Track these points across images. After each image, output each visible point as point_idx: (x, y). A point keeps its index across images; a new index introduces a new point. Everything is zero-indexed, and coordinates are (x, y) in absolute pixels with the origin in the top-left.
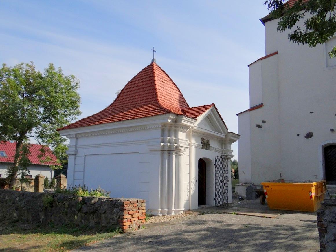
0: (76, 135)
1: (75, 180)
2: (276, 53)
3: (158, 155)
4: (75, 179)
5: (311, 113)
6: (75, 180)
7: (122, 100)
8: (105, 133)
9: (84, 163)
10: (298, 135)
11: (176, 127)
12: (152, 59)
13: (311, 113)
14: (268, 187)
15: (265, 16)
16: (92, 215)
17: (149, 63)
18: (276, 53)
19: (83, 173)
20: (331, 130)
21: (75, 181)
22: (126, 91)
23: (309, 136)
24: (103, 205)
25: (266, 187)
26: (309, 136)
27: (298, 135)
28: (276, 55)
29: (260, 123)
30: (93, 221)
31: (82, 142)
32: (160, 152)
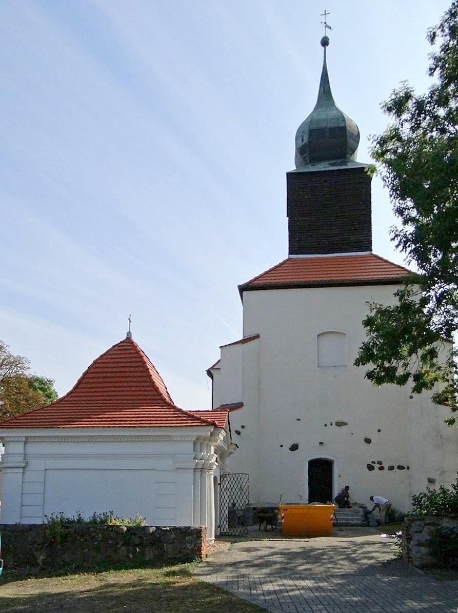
0: (26, 438)
1: (23, 505)
2: (257, 337)
3: (190, 475)
4: (23, 504)
5: (298, 420)
6: (23, 505)
7: (102, 390)
8: (91, 439)
9: (44, 482)
10: (282, 446)
11: (210, 440)
12: (128, 332)
13: (298, 420)
14: (287, 510)
15: (243, 283)
16: (150, 547)
17: (124, 338)
18: (257, 337)
19: (43, 495)
20: (320, 443)
21: (23, 507)
22: (91, 376)
23: (294, 448)
24: (168, 534)
25: (284, 510)
26: (294, 448)
27: (282, 446)
28: (256, 340)
29: (240, 429)
30: (150, 554)
31: (32, 449)
32: (192, 471)
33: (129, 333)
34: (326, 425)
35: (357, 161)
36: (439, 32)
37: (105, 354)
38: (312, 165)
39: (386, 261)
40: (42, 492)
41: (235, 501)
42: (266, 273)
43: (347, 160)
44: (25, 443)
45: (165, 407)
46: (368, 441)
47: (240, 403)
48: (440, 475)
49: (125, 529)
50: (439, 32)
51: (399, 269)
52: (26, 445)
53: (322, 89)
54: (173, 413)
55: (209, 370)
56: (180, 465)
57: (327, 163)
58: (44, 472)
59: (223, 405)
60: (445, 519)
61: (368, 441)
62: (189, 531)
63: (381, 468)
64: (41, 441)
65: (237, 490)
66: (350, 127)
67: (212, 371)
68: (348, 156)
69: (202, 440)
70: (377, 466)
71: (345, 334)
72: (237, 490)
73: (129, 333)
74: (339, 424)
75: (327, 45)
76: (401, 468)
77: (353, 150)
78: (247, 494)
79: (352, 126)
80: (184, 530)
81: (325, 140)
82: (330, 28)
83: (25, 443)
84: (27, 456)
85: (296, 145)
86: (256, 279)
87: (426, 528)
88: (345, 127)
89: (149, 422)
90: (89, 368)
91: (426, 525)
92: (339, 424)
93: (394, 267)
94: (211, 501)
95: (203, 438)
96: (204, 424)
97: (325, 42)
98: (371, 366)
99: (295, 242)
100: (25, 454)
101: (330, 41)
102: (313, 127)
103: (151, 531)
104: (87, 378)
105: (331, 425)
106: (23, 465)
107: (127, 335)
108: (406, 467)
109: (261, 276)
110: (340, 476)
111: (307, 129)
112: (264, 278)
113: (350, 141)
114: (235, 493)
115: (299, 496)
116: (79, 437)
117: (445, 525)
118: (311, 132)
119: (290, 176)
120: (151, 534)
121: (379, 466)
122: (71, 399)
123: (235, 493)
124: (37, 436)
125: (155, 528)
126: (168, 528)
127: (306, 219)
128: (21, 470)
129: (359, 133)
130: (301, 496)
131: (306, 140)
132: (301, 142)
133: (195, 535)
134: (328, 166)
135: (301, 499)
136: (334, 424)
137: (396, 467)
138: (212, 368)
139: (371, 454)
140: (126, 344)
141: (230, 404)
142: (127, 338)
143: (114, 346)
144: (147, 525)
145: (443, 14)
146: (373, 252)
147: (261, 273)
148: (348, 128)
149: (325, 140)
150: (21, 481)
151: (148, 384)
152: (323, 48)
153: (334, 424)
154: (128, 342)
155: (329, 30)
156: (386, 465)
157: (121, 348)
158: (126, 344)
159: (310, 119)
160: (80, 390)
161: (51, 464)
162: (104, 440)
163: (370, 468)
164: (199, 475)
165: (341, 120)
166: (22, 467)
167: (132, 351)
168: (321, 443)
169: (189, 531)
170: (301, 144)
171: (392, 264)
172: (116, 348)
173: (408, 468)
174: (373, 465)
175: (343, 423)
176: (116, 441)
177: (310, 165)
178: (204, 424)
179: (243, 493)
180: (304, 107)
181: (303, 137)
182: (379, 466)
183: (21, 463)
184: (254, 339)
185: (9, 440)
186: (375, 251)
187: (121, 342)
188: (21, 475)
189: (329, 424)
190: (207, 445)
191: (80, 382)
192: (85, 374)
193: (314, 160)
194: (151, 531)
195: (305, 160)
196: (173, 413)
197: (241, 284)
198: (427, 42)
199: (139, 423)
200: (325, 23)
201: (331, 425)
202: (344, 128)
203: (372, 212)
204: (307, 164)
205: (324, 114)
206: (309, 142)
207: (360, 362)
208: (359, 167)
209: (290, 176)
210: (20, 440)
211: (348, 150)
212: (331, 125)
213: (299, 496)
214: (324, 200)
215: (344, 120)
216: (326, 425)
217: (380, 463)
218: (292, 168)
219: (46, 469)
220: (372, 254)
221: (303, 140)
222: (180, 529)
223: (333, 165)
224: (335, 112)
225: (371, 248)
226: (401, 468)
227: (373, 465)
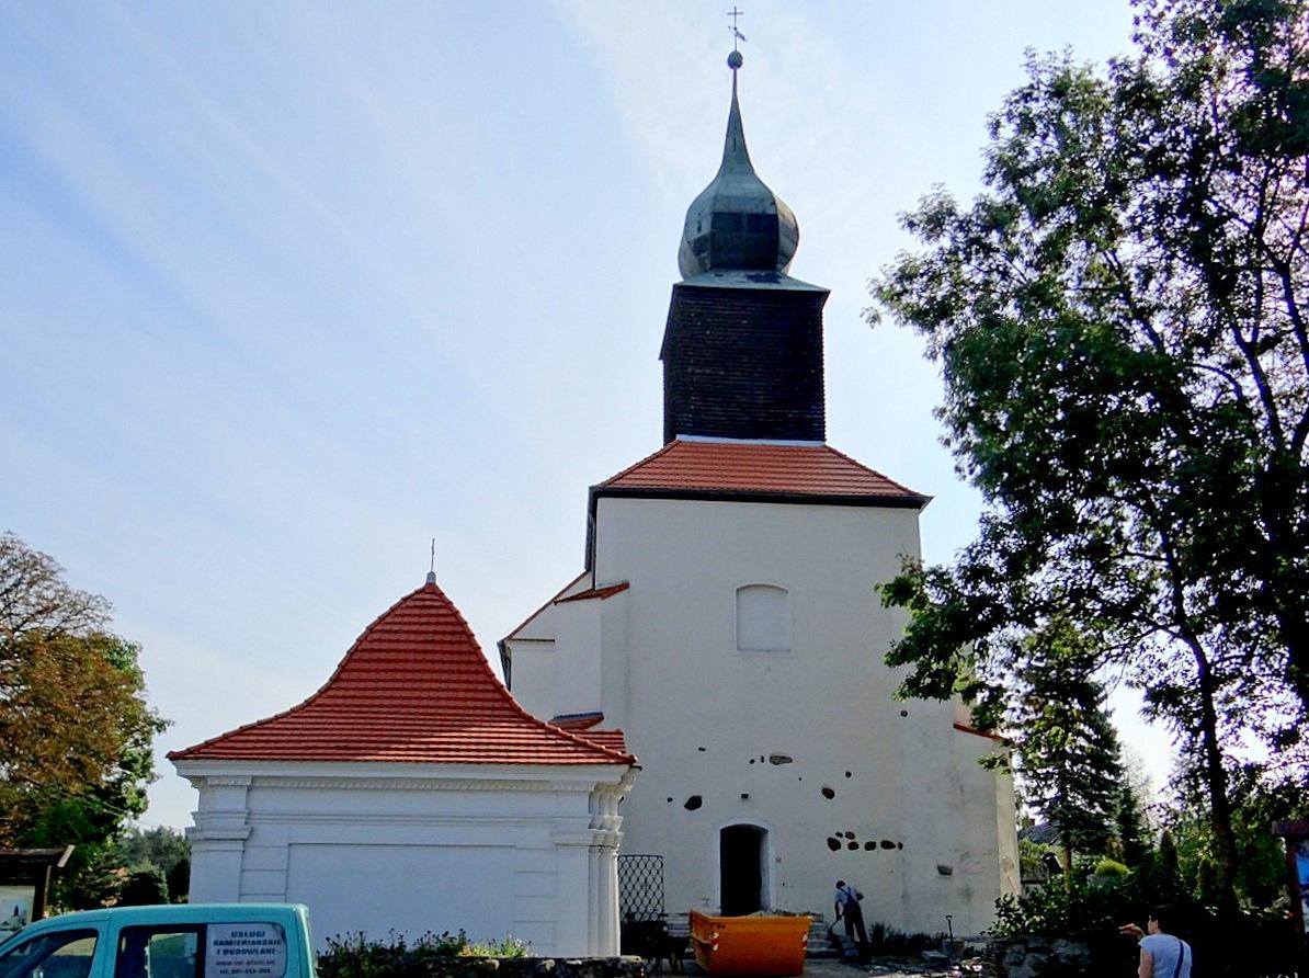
0: (254, 778)
2: (625, 586)
3: (582, 859)
8: (387, 785)
17: (421, 584)
18: (625, 586)
23: (694, 803)
26: (694, 803)
27: (670, 800)
31: (263, 801)
33: (432, 575)
34: (752, 762)
35: (789, 274)
36: (1003, 120)
37: (388, 615)
38: (718, 275)
39: (853, 462)
40: (283, 891)
41: (634, 909)
42: (639, 466)
43: (778, 273)
44: (249, 789)
45: (524, 725)
46: (829, 793)
47: (597, 714)
48: (962, 859)
49: (497, 963)
50: (1003, 120)
51: (876, 479)
52: (251, 793)
53: (732, 143)
54: (543, 737)
55: (503, 641)
56: (560, 839)
57: (742, 273)
58: (286, 850)
59: (561, 717)
60: (1062, 942)
61: (829, 793)
62: (619, 966)
63: (853, 846)
64: (269, 787)
65: (638, 887)
66: (784, 216)
67: (508, 644)
68: (779, 266)
69: (603, 791)
70: (845, 842)
71: (787, 592)
72: (638, 887)
73: (432, 575)
74: (778, 760)
75: (739, 66)
76: (887, 845)
77: (788, 257)
78: (659, 895)
79: (786, 215)
80: (610, 965)
81: (741, 236)
82: (743, 38)
83: (249, 789)
84: (252, 816)
85: (685, 231)
86: (622, 476)
87: (1029, 958)
88: (777, 215)
89: (504, 754)
90: (360, 641)
91: (1029, 950)
92: (778, 760)
93: (866, 473)
94: (615, 909)
95: (605, 787)
96: (612, 761)
97: (735, 61)
98: (910, 669)
99: (687, 412)
100: (250, 813)
101: (745, 61)
102: (720, 208)
103: (548, 968)
104: (355, 661)
105: (763, 760)
106: (245, 835)
107: (428, 578)
108: (896, 843)
109: (630, 471)
110: (779, 860)
111: (708, 209)
112: (637, 476)
113: (784, 241)
114: (634, 894)
115: (704, 899)
116: (363, 780)
117: (1060, 950)
118: (717, 217)
119: (676, 287)
120: (548, 973)
121: (850, 841)
122: (328, 701)
123: (634, 894)
124: (288, 777)
125: (553, 962)
126: (580, 962)
127: (708, 371)
128: (239, 846)
129: (797, 229)
130: (707, 900)
131: (706, 230)
132: (696, 232)
133: (631, 973)
134: (745, 280)
135: (707, 905)
136: (767, 759)
137: (878, 845)
138: (510, 638)
139: (835, 818)
140: (427, 596)
141: (577, 716)
142: (427, 583)
143: (405, 600)
144: (537, 956)
145: (1009, 93)
146: (827, 443)
147: (629, 466)
148: (780, 217)
149: (741, 236)
150: (239, 869)
151: (481, 677)
152: (732, 71)
153: (767, 759)
154: (431, 590)
155: (742, 41)
156: (861, 841)
157: (419, 603)
158: (427, 596)
159: (713, 194)
160: (343, 685)
161: (302, 833)
162: (400, 787)
163: (834, 845)
164: (597, 858)
165: (769, 202)
166: (242, 839)
167: (442, 611)
168: (745, 796)
169: (619, 966)
170: (697, 235)
171: (864, 468)
172: (409, 603)
173: (901, 846)
174: (838, 838)
175: (784, 758)
176: (468, 790)
177: (713, 275)
178: (612, 761)
179: (650, 894)
180: (701, 168)
181: (700, 223)
182: (850, 841)
183: (240, 830)
184: (619, 591)
185: (216, 782)
186: (835, 437)
187: (417, 592)
188: (240, 854)
189: (758, 760)
190: (610, 800)
191: (343, 668)
192: (351, 653)
193: (720, 266)
194: (548, 968)
195: (701, 262)
196: (543, 737)
197: (595, 484)
198: (987, 133)
199: (484, 755)
200: (735, 29)
201: (763, 760)
202: (775, 217)
203: (825, 371)
204: (706, 271)
205: (738, 188)
206: (713, 235)
207: (898, 657)
208: (795, 288)
209: (676, 287)
210: (240, 783)
211: (780, 257)
212: (750, 208)
213: (704, 899)
214: (743, 346)
215: (774, 203)
216: (752, 762)
217: (850, 835)
218: (679, 279)
219: (290, 844)
220: (825, 446)
221: (699, 229)
222: (601, 962)
223: (757, 279)
224: (754, 186)
225: (824, 436)
226: (887, 845)
227: (838, 838)
